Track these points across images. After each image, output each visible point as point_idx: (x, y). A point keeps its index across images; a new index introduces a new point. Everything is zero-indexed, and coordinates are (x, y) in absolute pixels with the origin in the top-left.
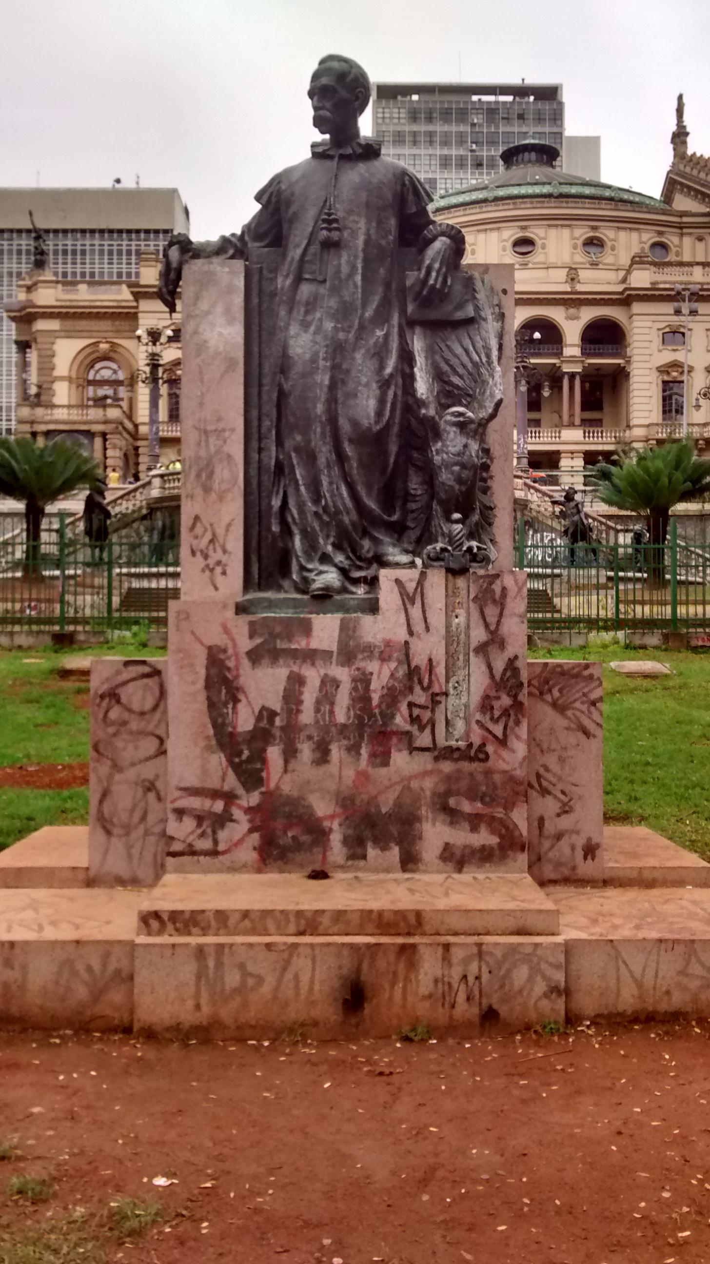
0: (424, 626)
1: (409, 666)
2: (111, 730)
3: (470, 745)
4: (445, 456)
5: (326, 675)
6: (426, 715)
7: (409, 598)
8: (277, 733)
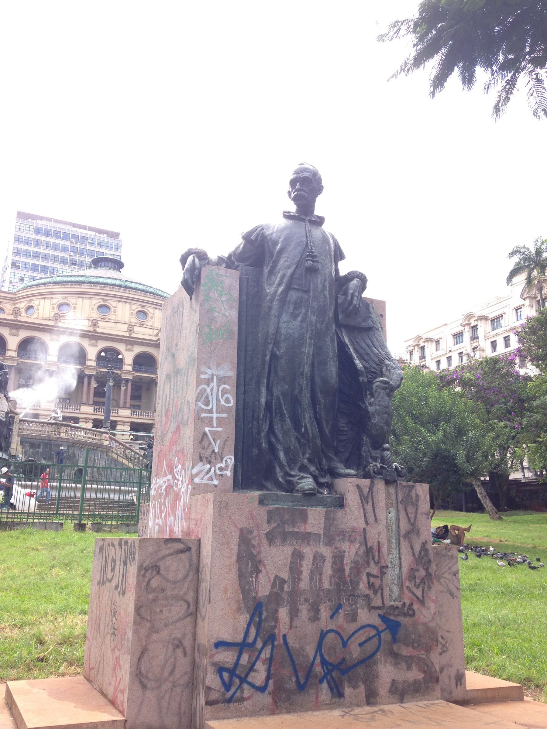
0: (373, 518)
1: (366, 546)
2: (151, 596)
3: (404, 604)
4: (378, 407)
5: (317, 551)
6: (377, 582)
7: (366, 498)
8: (285, 596)
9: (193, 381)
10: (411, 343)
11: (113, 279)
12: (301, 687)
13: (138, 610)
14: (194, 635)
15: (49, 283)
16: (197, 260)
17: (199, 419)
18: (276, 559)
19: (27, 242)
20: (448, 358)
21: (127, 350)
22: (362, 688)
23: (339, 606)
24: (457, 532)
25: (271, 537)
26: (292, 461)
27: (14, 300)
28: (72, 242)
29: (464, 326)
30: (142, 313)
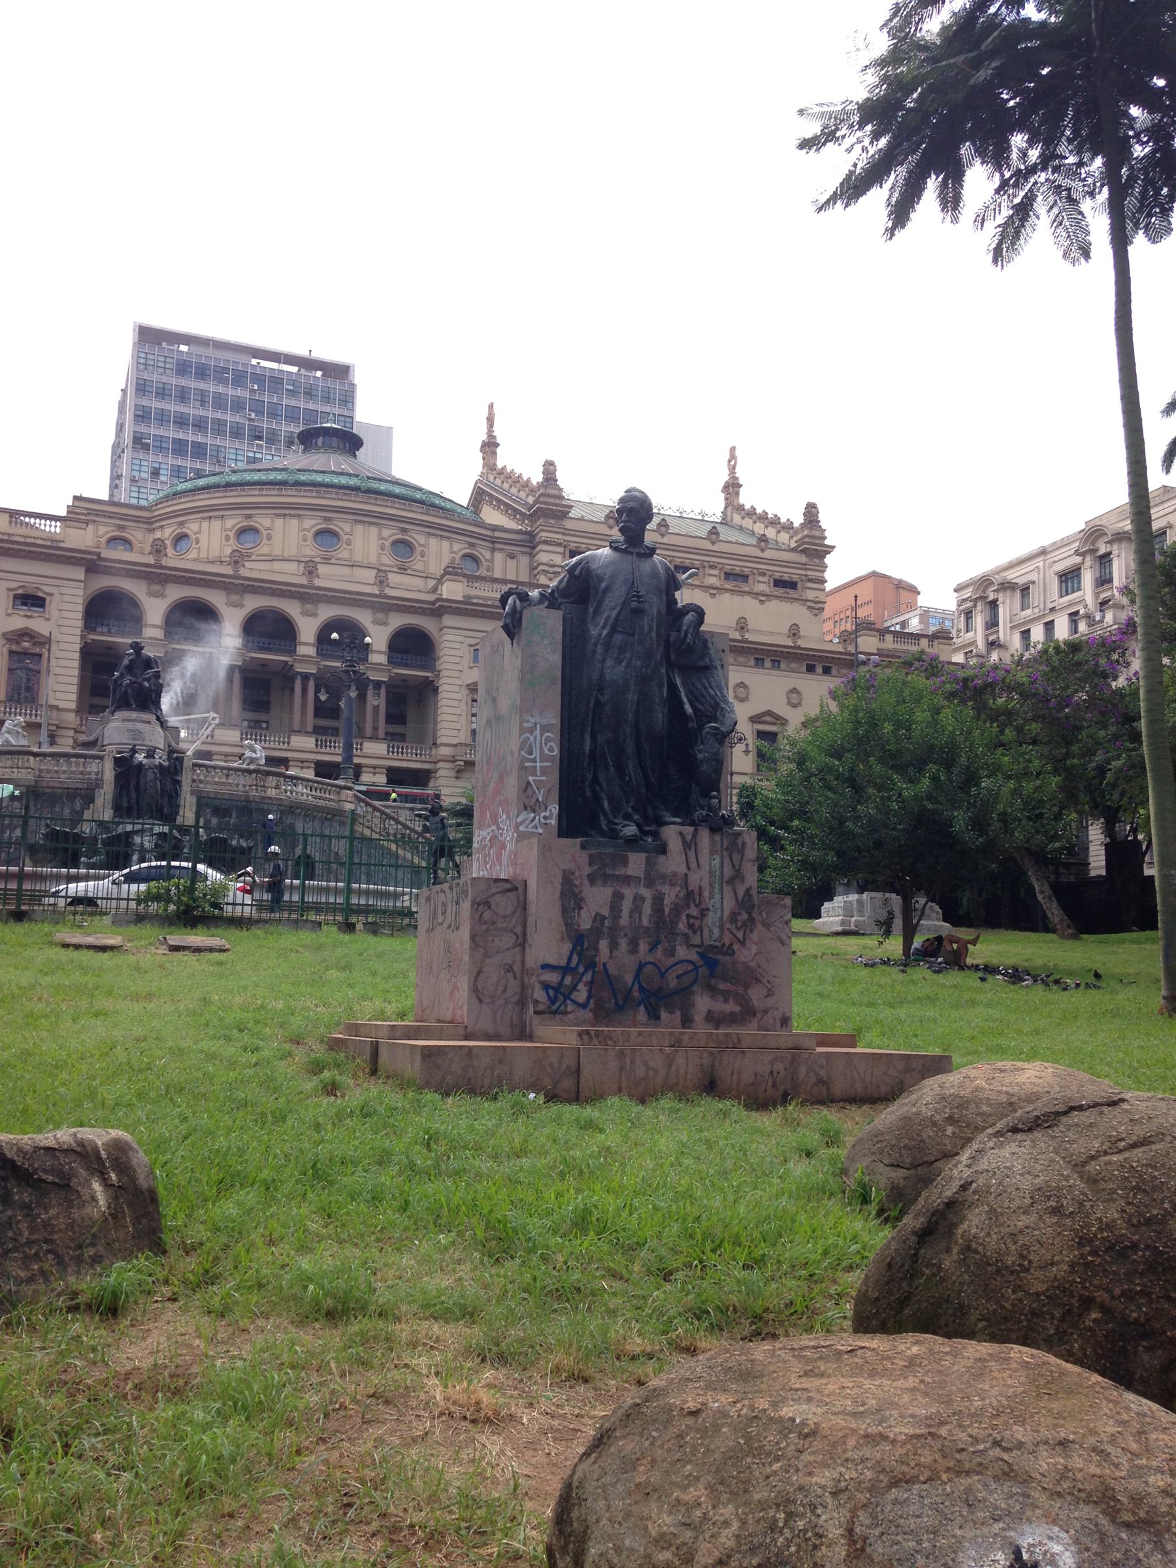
2: (484, 927)
6: (697, 923)
7: (689, 845)
8: (606, 931)
9: (515, 730)
10: (967, 593)
11: (342, 474)
12: (620, 1008)
13: (473, 938)
14: (523, 961)
15: (216, 486)
16: (518, 602)
17: (522, 768)
18: (597, 898)
19: (162, 394)
20: (1046, 624)
21: (376, 622)
22: (678, 1013)
23: (658, 943)
24: (955, 946)
25: (592, 879)
26: (616, 809)
27: (149, 523)
28: (253, 391)
29: (1083, 555)
30: (403, 547)
